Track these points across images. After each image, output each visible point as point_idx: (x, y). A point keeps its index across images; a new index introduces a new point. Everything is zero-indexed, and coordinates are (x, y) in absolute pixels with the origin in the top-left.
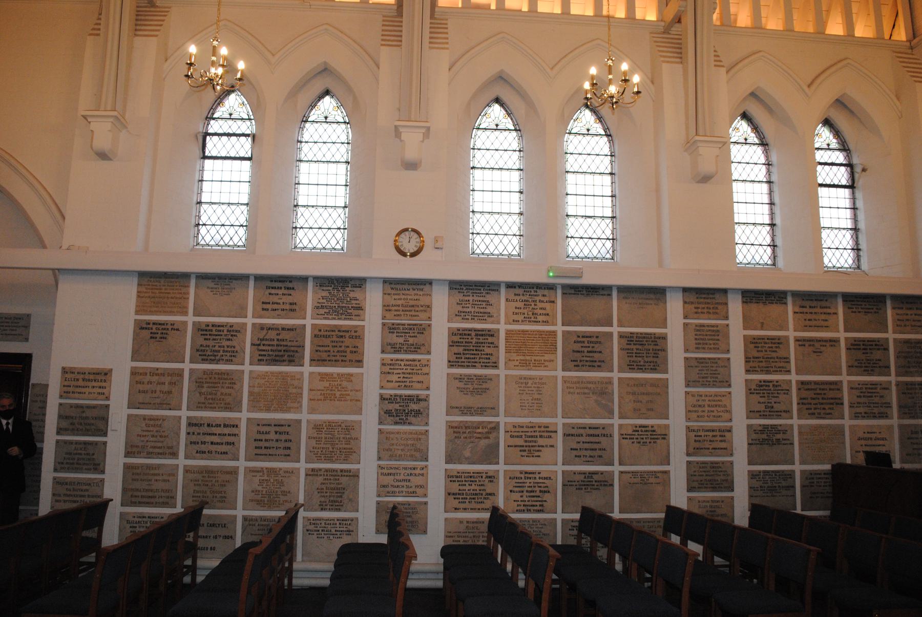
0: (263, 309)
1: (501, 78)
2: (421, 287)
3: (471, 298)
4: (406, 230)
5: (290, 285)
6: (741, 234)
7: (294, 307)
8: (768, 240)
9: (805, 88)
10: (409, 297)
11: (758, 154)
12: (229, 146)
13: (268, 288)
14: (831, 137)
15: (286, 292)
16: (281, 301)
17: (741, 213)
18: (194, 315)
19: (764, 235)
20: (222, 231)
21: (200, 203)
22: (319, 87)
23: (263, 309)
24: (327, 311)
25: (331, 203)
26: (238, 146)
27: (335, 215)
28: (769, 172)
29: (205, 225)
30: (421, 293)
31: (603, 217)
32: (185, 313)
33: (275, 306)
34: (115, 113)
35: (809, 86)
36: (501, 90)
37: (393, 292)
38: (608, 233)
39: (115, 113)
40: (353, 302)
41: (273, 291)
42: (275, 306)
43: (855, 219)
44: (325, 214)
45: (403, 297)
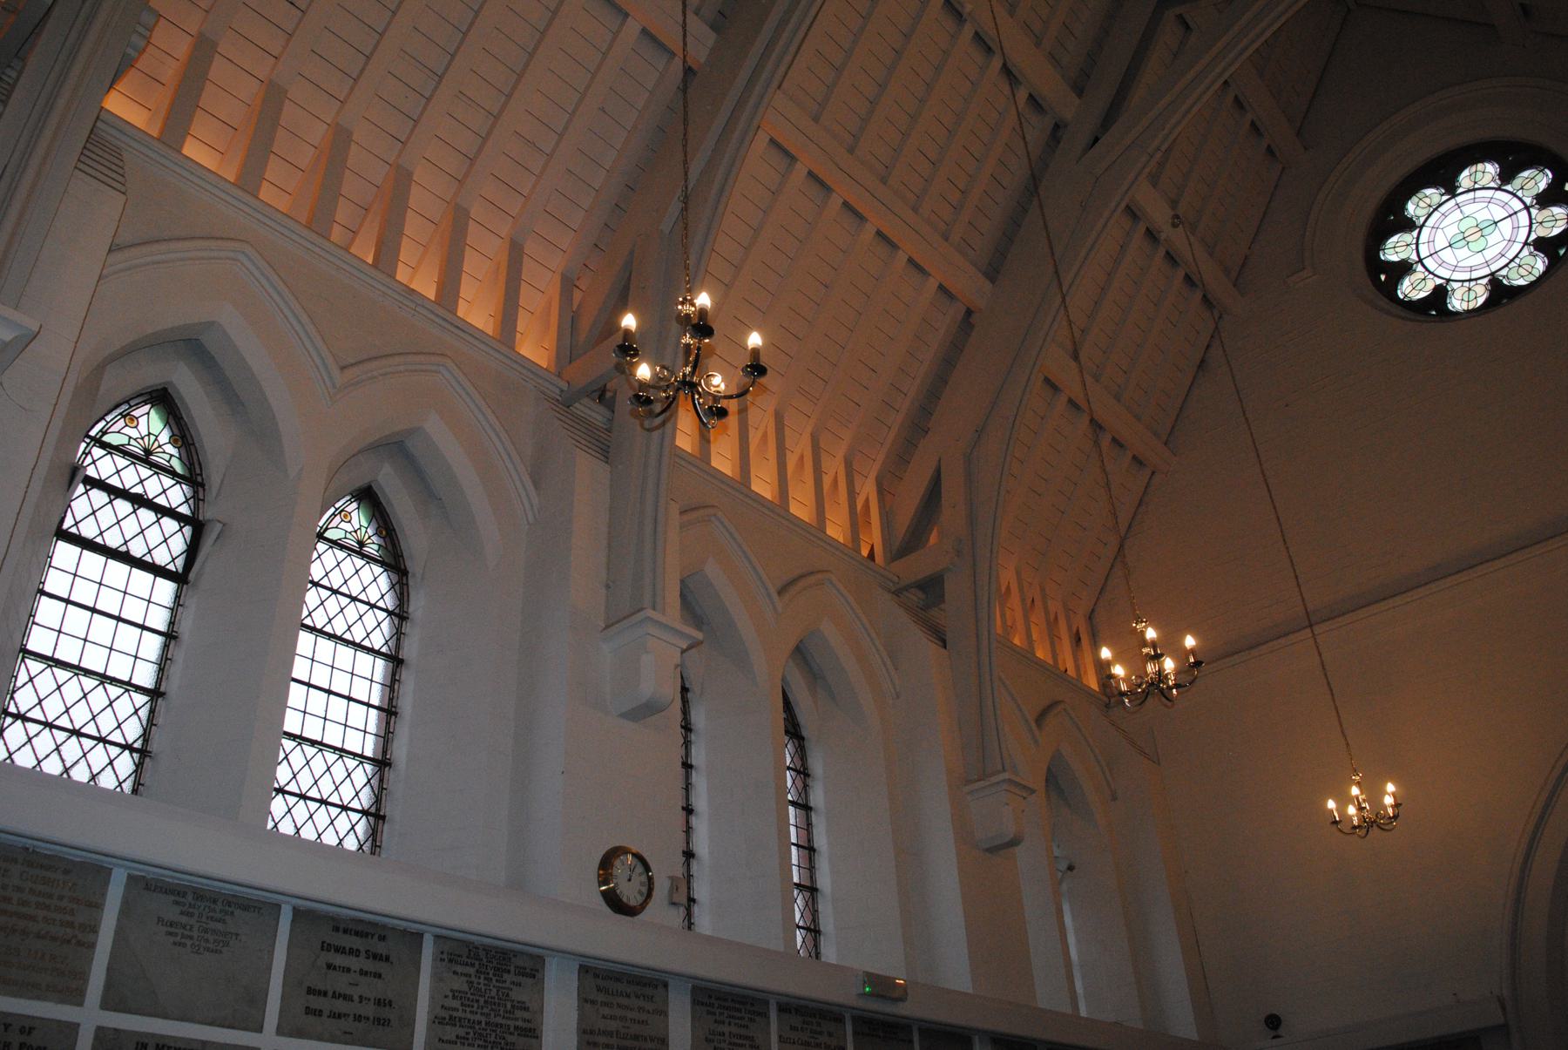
0: (308, 1011)
1: (193, 346)
2: (649, 991)
3: (726, 1029)
4: (647, 868)
5: (381, 948)
6: (294, 767)
7: (385, 1013)
8: (366, 799)
9: (775, 596)
10: (630, 1015)
11: (375, 583)
12: (130, 526)
13: (326, 947)
14: (164, 437)
15: (370, 965)
16: (355, 993)
17: (302, 711)
18: (107, 1004)
19: (356, 784)
20: (72, 749)
21: (154, 694)
22: (152, 374)
23: (308, 1011)
24: (461, 1032)
25: (120, 669)
26: (154, 536)
27: (124, 706)
28: (398, 635)
29: (24, 718)
30: (649, 1006)
31: (128, 686)
32: (76, 996)
33: (340, 1006)
34: (1006, 776)
35: (779, 593)
36: (181, 377)
37: (601, 998)
38: (133, 731)
39: (1006, 776)
40: (519, 1014)
41: (339, 960)
42: (340, 1006)
43: (386, 737)
44: (98, 698)
45: (618, 1012)
